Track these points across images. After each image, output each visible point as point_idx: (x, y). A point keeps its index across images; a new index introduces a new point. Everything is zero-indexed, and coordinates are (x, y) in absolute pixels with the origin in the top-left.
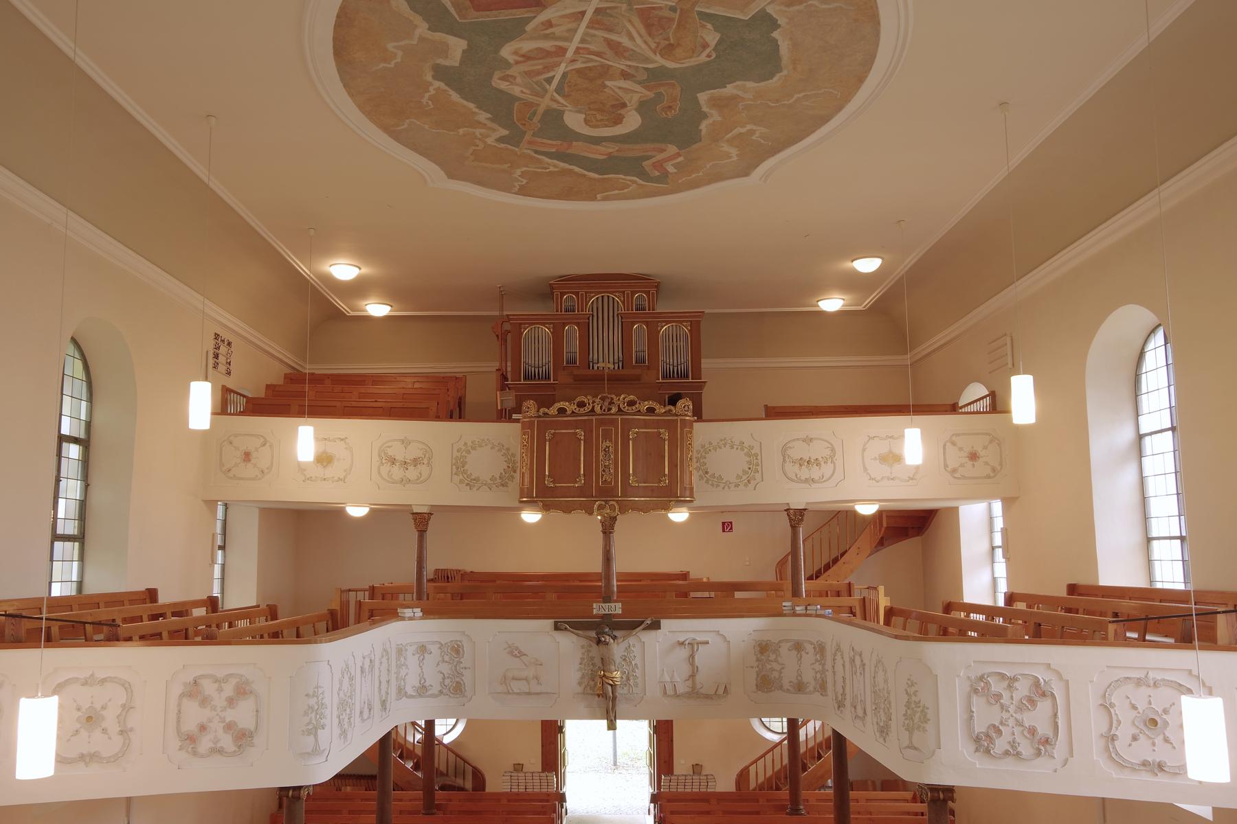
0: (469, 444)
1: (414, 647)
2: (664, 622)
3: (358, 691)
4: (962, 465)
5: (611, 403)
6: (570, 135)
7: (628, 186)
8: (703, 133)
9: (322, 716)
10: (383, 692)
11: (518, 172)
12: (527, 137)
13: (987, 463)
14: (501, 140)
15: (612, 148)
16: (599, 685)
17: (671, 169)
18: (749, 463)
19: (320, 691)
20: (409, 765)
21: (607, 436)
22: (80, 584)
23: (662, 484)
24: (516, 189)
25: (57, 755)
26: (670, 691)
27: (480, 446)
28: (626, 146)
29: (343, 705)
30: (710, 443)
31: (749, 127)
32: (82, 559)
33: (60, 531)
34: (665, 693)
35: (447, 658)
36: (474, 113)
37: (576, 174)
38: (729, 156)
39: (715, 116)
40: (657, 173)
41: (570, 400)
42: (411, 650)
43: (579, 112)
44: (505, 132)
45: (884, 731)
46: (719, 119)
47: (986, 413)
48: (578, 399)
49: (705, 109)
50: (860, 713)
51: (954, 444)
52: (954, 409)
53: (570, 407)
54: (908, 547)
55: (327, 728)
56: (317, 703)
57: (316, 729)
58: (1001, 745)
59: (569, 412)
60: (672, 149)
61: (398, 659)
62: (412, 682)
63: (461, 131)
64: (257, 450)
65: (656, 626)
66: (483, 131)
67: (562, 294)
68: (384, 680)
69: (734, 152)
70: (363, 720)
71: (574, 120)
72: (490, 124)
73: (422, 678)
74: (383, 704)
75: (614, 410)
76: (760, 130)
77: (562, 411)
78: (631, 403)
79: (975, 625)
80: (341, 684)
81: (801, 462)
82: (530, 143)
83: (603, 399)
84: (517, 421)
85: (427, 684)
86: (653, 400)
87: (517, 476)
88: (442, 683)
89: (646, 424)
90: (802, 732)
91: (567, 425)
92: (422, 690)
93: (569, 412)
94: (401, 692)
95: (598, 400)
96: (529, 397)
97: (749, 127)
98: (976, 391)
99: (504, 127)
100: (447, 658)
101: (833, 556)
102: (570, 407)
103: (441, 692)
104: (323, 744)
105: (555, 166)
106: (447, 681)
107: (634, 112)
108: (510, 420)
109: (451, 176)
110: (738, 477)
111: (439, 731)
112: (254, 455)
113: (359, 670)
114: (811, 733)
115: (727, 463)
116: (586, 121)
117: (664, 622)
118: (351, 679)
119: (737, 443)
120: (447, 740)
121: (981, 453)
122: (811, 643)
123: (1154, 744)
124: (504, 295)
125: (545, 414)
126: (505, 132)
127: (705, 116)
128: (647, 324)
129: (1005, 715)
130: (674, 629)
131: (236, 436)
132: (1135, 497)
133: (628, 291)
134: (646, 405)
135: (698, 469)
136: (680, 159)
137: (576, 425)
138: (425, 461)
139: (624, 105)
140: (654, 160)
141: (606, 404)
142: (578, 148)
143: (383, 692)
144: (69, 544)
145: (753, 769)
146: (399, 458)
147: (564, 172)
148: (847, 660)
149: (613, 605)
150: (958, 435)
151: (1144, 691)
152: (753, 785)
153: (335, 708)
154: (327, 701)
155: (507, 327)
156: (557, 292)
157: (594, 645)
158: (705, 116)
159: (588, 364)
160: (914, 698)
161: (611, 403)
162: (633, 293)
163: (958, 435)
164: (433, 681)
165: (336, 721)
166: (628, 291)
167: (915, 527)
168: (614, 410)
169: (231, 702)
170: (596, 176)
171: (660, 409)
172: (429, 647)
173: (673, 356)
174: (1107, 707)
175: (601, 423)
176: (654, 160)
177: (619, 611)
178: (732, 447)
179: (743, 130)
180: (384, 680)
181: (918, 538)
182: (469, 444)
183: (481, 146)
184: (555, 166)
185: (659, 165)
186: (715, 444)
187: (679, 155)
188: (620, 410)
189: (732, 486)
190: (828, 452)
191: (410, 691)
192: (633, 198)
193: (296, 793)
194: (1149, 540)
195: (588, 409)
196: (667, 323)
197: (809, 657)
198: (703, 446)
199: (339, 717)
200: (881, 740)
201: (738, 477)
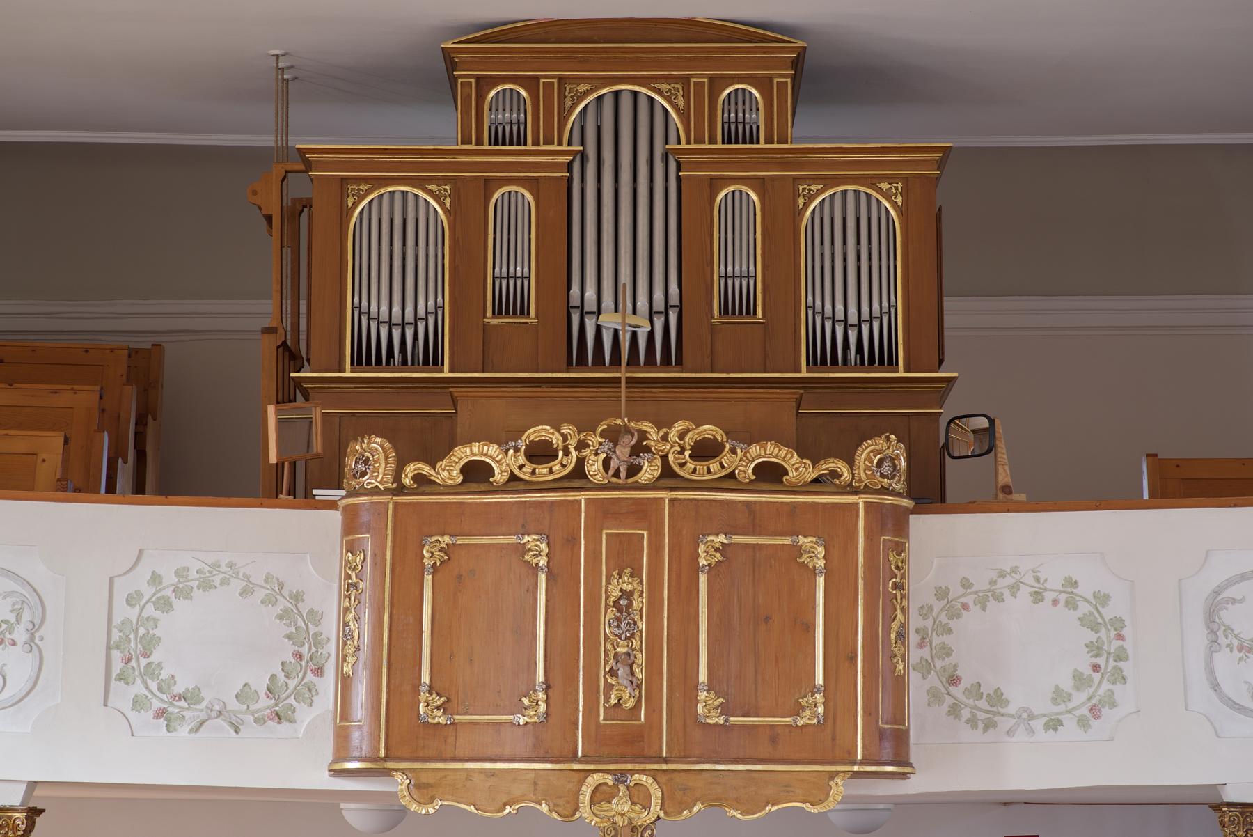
0: (169, 578)
5: (640, 449)
18: (1096, 649)
21: (625, 557)
23: (804, 719)
25: (77, 483)
27: (206, 585)
30: (966, 584)
41: (504, 438)
48: (540, 432)
53: (503, 461)
59: (500, 477)
67: (483, 84)
75: (649, 470)
77: (476, 473)
78: (705, 451)
83: (613, 436)
84: (331, 505)
86: (781, 441)
87: (328, 686)
89: (754, 520)
91: (493, 520)
93: (500, 477)
95: (594, 440)
102: (503, 461)
108: (309, 502)
110: (1059, 696)
119: (1055, 582)
124: (287, 83)
125: (419, 478)
128: (761, 185)
133: (700, 77)
134: (743, 461)
135: (926, 668)
137: (524, 521)
138: (20, 635)
141: (623, 451)
155: (298, 188)
156: (465, 76)
159: (567, 312)
161: (640, 449)
162: (716, 84)
166: (700, 77)
168: (649, 470)
171: (798, 469)
173: (852, 291)
175: (604, 512)
178: (1038, 597)
182: (169, 578)
186: (980, 584)
189: (1038, 724)
195: (560, 468)
198: (942, 593)
201: (1059, 696)
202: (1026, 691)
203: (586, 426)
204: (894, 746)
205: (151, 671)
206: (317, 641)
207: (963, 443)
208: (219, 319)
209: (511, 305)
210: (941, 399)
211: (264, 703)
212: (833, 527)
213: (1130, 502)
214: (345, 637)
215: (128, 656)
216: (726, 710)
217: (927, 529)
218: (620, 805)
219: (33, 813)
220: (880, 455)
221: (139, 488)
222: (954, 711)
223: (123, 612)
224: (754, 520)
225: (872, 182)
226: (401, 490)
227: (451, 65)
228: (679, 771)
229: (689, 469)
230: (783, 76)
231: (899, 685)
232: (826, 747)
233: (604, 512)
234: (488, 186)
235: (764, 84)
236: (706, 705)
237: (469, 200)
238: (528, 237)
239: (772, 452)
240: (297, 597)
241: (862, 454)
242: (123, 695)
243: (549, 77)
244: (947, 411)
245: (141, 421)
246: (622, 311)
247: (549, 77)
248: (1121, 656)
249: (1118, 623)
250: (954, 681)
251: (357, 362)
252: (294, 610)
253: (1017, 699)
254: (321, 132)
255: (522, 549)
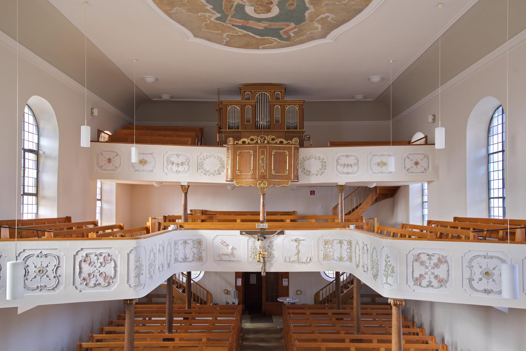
0: (205, 156)
1: (182, 241)
2: (287, 232)
3: (157, 259)
4: (412, 167)
6: (248, 18)
7: (273, 43)
8: (306, 17)
9: (142, 270)
10: (168, 260)
11: (225, 35)
12: (229, 18)
13: (422, 166)
14: (217, 19)
15: (266, 24)
16: (258, 257)
17: (292, 35)
18: (322, 165)
19: (141, 259)
20: (181, 291)
21: (263, 153)
22: (37, 213)
24: (225, 43)
25: (193, 144)
26: (288, 260)
27: (210, 157)
28: (272, 23)
29: (151, 265)
31: (327, 14)
32: (37, 204)
33: (26, 191)
34: (285, 261)
35: (195, 246)
36: (205, 5)
37: (250, 36)
38: (317, 28)
39: (312, 9)
40: (286, 36)
41: (247, 138)
42: (180, 242)
43: (252, 6)
44: (219, 15)
45: (375, 276)
46: (314, 10)
47: (423, 145)
48: (252, 137)
49: (307, 5)
50: (366, 270)
51: (408, 158)
52: (409, 143)
53: (247, 141)
54: (387, 202)
55: (144, 275)
56: (139, 264)
57: (139, 275)
58: (425, 283)
59: (247, 143)
60: (293, 25)
61: (175, 246)
62: (181, 256)
63: (199, 14)
64: (114, 157)
65: (282, 233)
66: (209, 14)
67: (245, 92)
68: (169, 254)
69: (319, 26)
70: (160, 272)
71: (249, 10)
72: (212, 11)
73: (185, 254)
74: (169, 265)
76: (331, 16)
77: (244, 142)
79: (415, 234)
80: (150, 257)
81: (344, 165)
82: (230, 21)
83: (261, 137)
85: (187, 257)
87: (225, 170)
88: (194, 256)
89: (279, 148)
90: (341, 277)
92: (185, 259)
93: (247, 143)
94: (176, 260)
96: (230, 137)
97: (327, 14)
98: (419, 136)
99: (219, 12)
100: (195, 246)
101: (353, 208)
102: (247, 141)
103: (193, 260)
104: (142, 282)
105: (241, 32)
106: (196, 256)
107: (276, 7)
109: (195, 36)
110: (318, 171)
111: (193, 277)
112: (112, 160)
113: (158, 250)
114: (345, 278)
115: (314, 166)
116: (255, 11)
117: (287, 232)
118: (154, 254)
119: (317, 157)
120: (196, 280)
121: (420, 162)
122: (346, 241)
123: (488, 282)
124: (219, 92)
125: (237, 143)
126: (219, 15)
127: (307, 9)
128: (280, 105)
129: (427, 270)
130: (291, 234)
131: (104, 151)
132: (485, 180)
133: (273, 91)
134: (278, 141)
135: (301, 168)
136: (296, 30)
137: (250, 148)
138: (187, 163)
139: (272, 3)
140: (285, 30)
141: (262, 139)
142: (251, 24)
143: (168, 260)
144: (30, 197)
145: (321, 292)
146: (176, 162)
147: (245, 35)
148: (361, 248)
149: (264, 224)
150: (410, 154)
151: (486, 260)
152: (321, 299)
153: (147, 266)
154: (144, 263)
155: (221, 106)
157: (257, 241)
158: (307, 9)
159: (255, 122)
160: (389, 263)
162: (275, 92)
163: (410, 154)
164: (190, 256)
165: (148, 272)
166: (273, 91)
167: (390, 193)
169: (436, 265)
170: (259, 37)
171: (285, 142)
172: (188, 241)
173: (292, 120)
174: (471, 267)
176: (285, 30)
177: (267, 227)
178: (315, 159)
179: (324, 16)
180: (169, 254)
181: (391, 199)
182: (205, 156)
183: (209, 22)
184: (241, 32)
185: (287, 33)
186: (308, 157)
187: (295, 28)
188: (268, 142)
190: (356, 161)
191: (180, 260)
192: (275, 48)
193: (131, 302)
194: (490, 198)
196: (289, 105)
197: (345, 246)
198: (303, 158)
199: (149, 270)
200: (374, 280)
201: (318, 171)
202: (314, 171)
203: (258, 136)
204: (297, 177)
205: (203, 168)
206: (224, 164)
207: (306, 139)
208: (211, 124)
209: (248, 121)
210: (303, 133)
211: (217, 172)
212: (289, 149)
213: (328, 147)
214: (227, 164)
215: (200, 166)
216: (276, 173)
217: (301, 150)
218: (262, 185)
219: (189, 186)
220: (295, 140)
221: (201, 145)
222: (304, 173)
223: (199, 160)
224: (279, 148)
225: (295, 105)
226: (234, 144)
227: (240, 89)
228: (263, 202)
229: (271, 142)
230: (283, 91)
231: (298, 170)
232: (288, 178)
233: (260, 147)
234: (245, 105)
235: (281, 92)
236: (273, 172)
237: (243, 107)
238: (250, 112)
239: (281, 140)
240: (221, 159)
241: (293, 140)
242: (200, 171)
243: (253, 91)
244: (304, 135)
245: (201, 137)
246: (262, 122)
247: (253, 91)
248: (326, 166)
249: (325, 162)
250: (304, 169)
251: (229, 129)
252: (221, 160)
253: (312, 172)
254: (224, 98)
255: (250, 152)
